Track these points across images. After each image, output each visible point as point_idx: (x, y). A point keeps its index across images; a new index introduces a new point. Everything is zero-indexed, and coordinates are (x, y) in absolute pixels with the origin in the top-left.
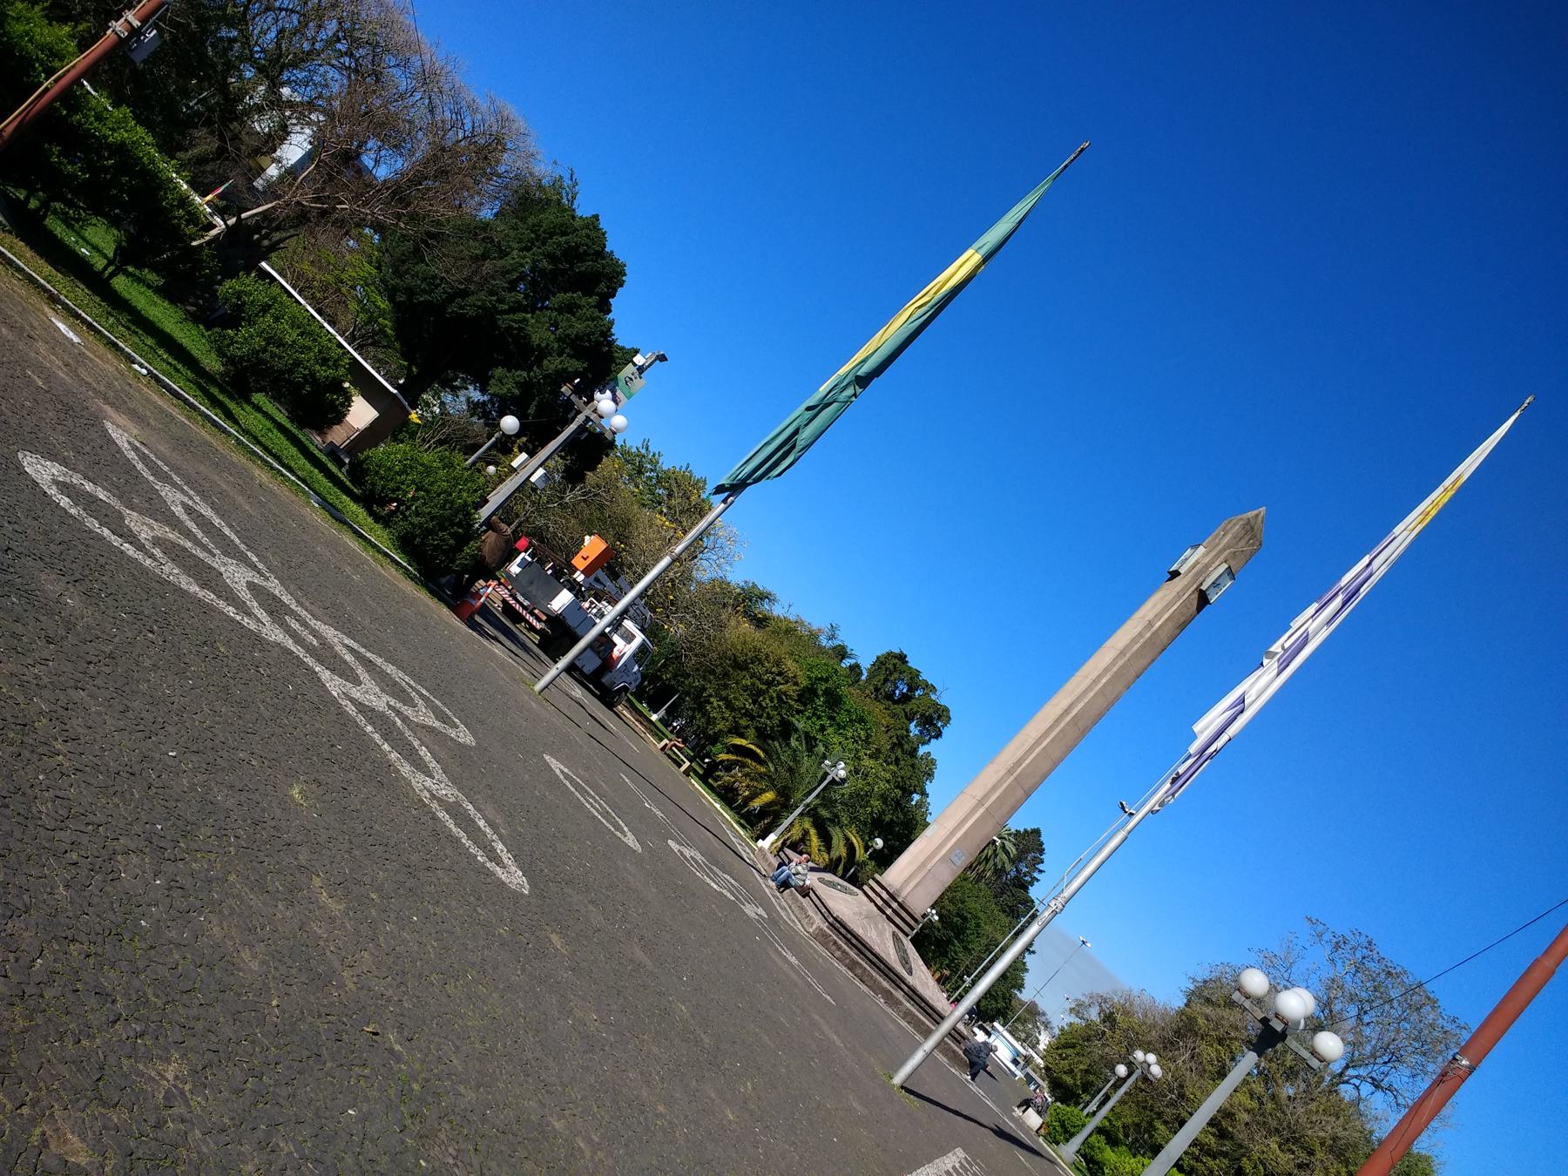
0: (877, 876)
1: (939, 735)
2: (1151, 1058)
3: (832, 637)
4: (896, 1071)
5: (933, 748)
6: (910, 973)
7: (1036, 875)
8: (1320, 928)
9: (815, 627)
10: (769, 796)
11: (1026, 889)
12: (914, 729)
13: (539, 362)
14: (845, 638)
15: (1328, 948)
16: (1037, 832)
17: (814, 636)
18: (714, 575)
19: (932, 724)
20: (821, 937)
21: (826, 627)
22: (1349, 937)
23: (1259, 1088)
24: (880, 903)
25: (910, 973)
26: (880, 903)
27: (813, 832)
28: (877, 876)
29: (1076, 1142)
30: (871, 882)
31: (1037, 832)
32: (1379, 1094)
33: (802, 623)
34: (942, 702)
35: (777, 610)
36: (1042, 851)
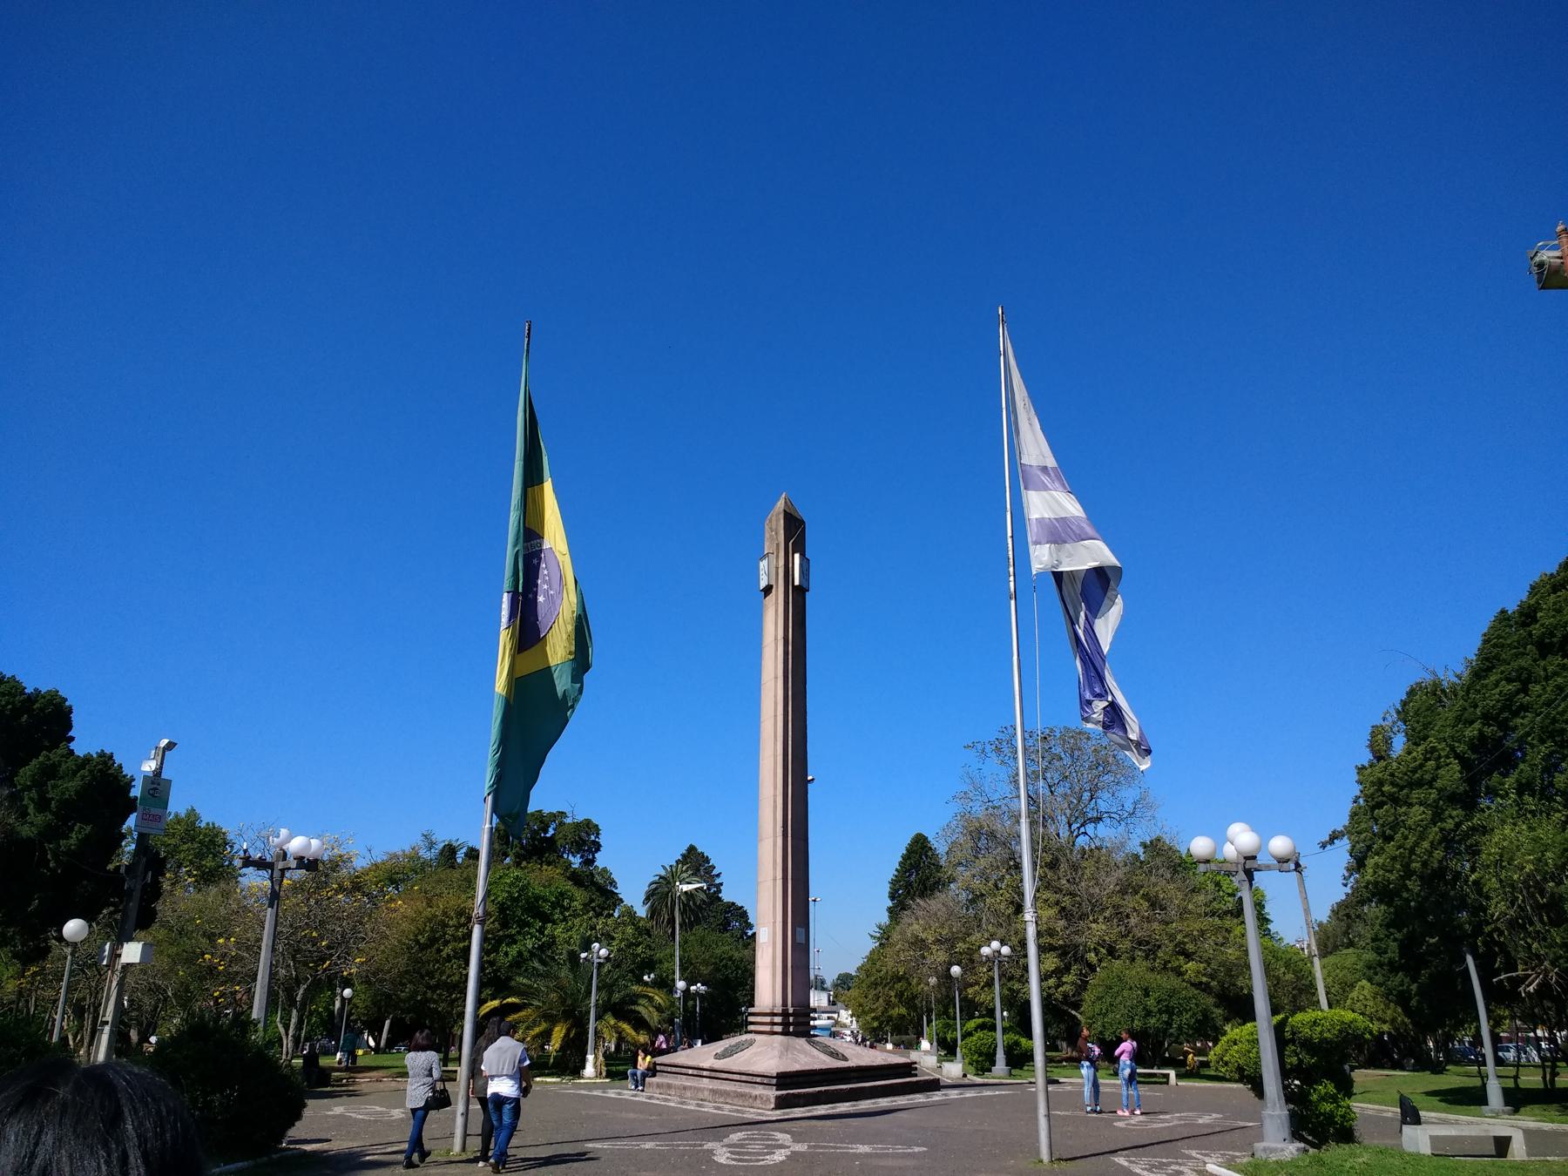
0: (751, 1010)
1: (598, 847)
2: (995, 944)
3: (431, 845)
4: (1038, 1152)
5: (601, 860)
6: (846, 1059)
7: (718, 881)
8: (979, 747)
9: (407, 849)
10: (558, 1034)
11: (720, 899)
12: (576, 861)
13: (517, 856)
14: (442, 838)
15: (994, 755)
16: (692, 849)
17: (414, 857)
18: (932, 902)
19: (584, 842)
20: (781, 1103)
21: (418, 840)
22: (1001, 736)
23: (1047, 895)
24: (767, 1028)
25: (846, 1059)
26: (767, 1028)
27: (626, 1027)
28: (751, 1010)
29: (1000, 1056)
30: (751, 1019)
31: (692, 849)
32: (1101, 825)
33: (396, 856)
34: (580, 818)
35: (360, 863)
36: (707, 860)
